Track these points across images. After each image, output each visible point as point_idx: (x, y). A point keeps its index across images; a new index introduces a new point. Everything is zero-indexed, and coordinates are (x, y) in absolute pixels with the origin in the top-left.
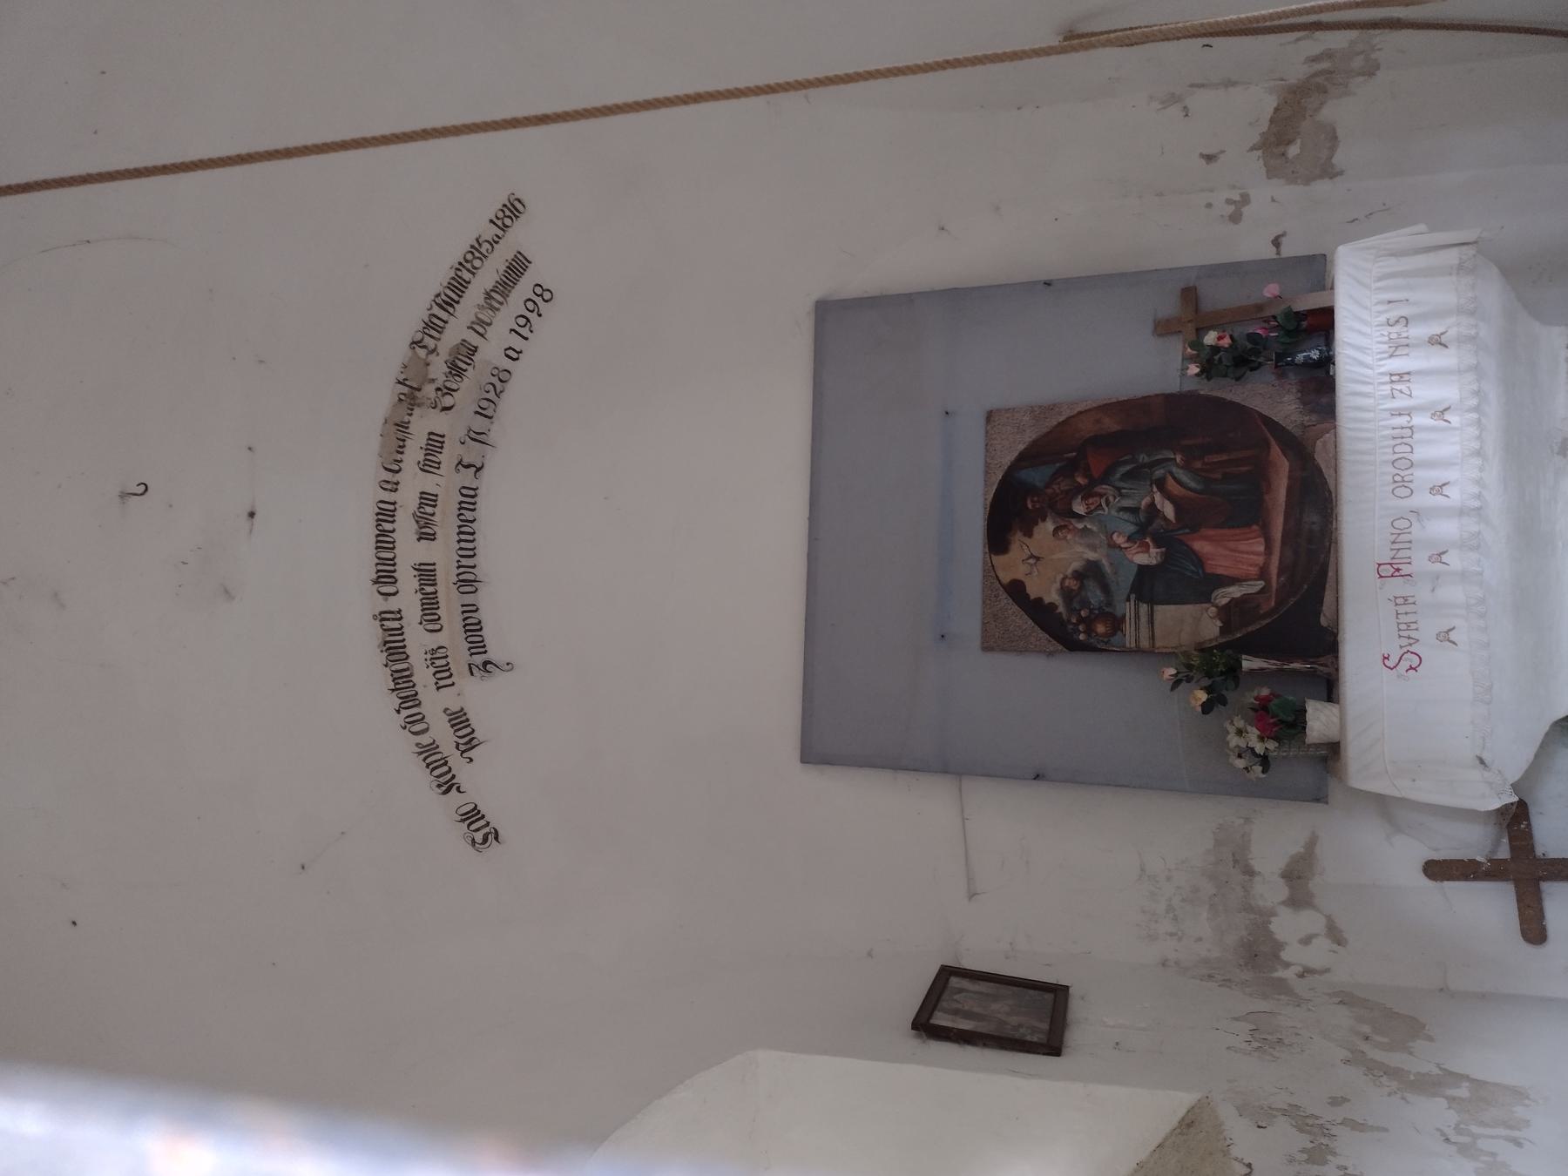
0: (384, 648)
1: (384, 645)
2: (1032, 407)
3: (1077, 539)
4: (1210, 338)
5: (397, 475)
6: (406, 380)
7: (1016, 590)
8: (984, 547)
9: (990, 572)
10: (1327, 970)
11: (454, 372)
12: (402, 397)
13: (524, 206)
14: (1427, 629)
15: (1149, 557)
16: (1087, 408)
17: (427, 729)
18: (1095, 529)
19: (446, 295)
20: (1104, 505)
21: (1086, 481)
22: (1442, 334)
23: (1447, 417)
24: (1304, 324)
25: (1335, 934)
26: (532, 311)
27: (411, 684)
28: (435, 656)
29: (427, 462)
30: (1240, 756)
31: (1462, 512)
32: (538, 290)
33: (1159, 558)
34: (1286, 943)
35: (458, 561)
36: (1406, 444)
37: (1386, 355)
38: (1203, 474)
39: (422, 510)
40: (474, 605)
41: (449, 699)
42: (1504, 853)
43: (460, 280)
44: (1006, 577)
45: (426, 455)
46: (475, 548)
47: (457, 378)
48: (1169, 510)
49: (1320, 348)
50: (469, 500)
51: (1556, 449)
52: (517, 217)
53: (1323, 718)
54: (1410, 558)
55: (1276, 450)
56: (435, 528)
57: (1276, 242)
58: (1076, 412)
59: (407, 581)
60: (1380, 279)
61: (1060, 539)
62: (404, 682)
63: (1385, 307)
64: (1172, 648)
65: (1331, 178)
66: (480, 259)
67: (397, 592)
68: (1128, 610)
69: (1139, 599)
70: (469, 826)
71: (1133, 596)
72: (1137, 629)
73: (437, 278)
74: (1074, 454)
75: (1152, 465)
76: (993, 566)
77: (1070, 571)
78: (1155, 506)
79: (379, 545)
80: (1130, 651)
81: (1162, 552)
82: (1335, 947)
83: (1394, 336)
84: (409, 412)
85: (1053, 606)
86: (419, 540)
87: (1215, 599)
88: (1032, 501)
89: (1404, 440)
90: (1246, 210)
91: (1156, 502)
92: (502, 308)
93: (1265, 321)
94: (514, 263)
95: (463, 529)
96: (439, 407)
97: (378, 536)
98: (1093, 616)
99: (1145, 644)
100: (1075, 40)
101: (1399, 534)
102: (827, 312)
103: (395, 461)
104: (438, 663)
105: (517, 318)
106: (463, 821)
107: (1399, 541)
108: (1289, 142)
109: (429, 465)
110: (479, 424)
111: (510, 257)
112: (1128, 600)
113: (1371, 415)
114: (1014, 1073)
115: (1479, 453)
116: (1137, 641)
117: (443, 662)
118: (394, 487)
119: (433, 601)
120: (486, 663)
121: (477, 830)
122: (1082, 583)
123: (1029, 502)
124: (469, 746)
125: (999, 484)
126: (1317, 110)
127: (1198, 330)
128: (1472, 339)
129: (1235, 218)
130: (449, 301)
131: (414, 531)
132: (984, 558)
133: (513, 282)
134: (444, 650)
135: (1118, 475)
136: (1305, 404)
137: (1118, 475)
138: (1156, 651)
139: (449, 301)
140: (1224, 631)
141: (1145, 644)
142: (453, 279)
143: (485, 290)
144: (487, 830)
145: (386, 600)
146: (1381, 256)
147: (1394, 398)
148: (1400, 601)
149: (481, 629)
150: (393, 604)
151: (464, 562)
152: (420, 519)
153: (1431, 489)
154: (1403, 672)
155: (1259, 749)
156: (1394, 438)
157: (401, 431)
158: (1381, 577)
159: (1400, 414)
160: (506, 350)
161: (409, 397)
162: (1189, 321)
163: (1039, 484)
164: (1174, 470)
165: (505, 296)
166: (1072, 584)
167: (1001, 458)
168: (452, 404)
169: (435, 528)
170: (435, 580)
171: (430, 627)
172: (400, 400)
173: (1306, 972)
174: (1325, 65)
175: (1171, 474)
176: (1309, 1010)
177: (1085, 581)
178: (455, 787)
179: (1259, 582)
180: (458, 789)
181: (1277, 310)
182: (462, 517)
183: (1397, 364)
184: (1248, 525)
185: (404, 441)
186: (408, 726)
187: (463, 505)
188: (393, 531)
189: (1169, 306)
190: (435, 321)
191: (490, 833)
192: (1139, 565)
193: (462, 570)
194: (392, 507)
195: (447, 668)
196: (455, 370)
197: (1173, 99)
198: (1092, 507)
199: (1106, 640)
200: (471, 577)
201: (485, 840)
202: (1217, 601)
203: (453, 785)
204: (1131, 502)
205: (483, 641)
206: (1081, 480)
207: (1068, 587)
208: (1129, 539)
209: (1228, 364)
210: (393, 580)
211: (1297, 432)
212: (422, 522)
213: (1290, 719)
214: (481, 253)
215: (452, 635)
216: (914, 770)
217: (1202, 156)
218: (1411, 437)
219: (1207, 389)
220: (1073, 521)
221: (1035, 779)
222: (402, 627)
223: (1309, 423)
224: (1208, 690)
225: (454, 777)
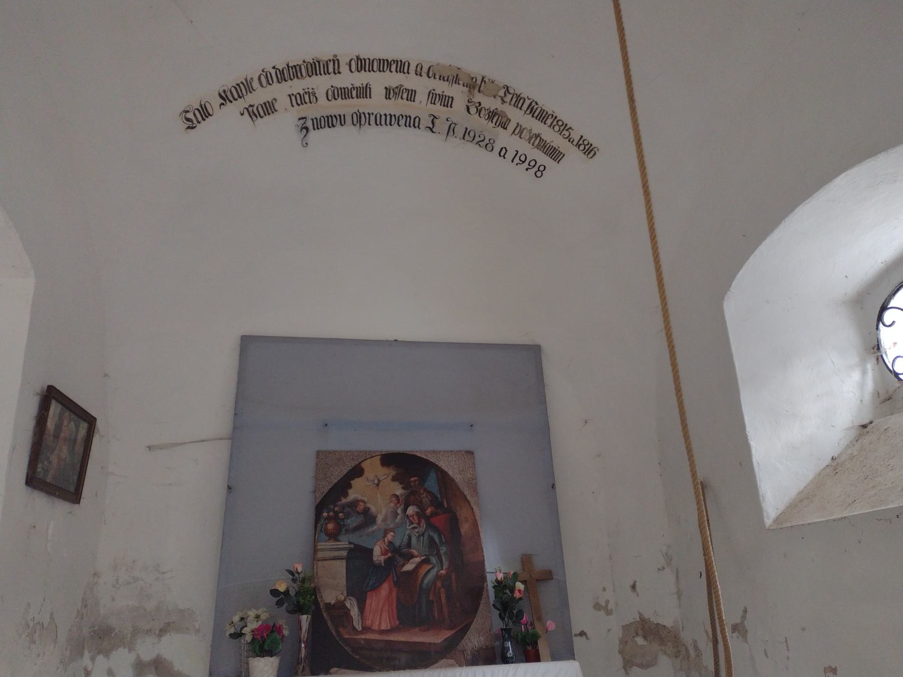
0: (315, 61)
1: (317, 61)
2: (476, 479)
3: (390, 510)
4: (520, 586)
5: (426, 75)
6: (485, 82)
7: (357, 471)
8: (385, 452)
9: (370, 455)
11: (491, 114)
12: (474, 80)
13: (592, 157)
15: (378, 556)
17: (262, 86)
18: (397, 521)
19: (537, 109)
20: (413, 526)
21: (428, 514)
24: (530, 648)
26: (529, 165)
27: (292, 78)
28: (311, 94)
29: (434, 95)
30: (242, 619)
32: (542, 168)
35: (373, 114)
39: (404, 91)
40: (345, 123)
41: (283, 102)
43: (546, 117)
44: (364, 465)
45: (439, 95)
46: (381, 125)
47: (487, 116)
48: (409, 567)
49: (514, 657)
50: (412, 122)
52: (585, 153)
53: (266, 669)
55: (448, 634)
56: (393, 99)
57: (582, 634)
58: (472, 506)
59: (360, 79)
61: (390, 499)
62: (293, 72)
64: (317, 573)
65: (624, 667)
66: (559, 130)
67: (352, 72)
68: (343, 543)
70: (198, 110)
71: (352, 546)
72: (331, 550)
73: (547, 103)
76: (373, 457)
77: (369, 505)
78: (412, 559)
79: (382, 61)
80: (315, 546)
81: (381, 563)
84: (465, 85)
85: (346, 495)
86: (386, 88)
87: (349, 599)
88: (415, 481)
92: (531, 145)
93: (531, 623)
94: (557, 152)
95: (393, 117)
96: (469, 104)
97: (387, 60)
99: (320, 555)
100: (701, 489)
102: (534, 351)
103: (435, 74)
104: (307, 97)
105: (525, 155)
106: (201, 106)
108: (645, 637)
109: (433, 97)
110: (460, 131)
111: (561, 150)
112: (350, 543)
114: (13, 448)
116: (322, 550)
117: (307, 100)
118: (418, 73)
119: (347, 95)
120: (307, 129)
121: (194, 114)
123: (415, 478)
124: (251, 114)
125: (427, 460)
126: (665, 653)
127: (526, 581)
129: (597, 607)
130: (534, 110)
131: (391, 85)
132: (379, 452)
133: (546, 152)
134: (315, 101)
135: (432, 534)
137: (432, 534)
139: (534, 110)
140: (328, 606)
141: (320, 555)
142: (547, 113)
143: (541, 134)
144: (195, 121)
145: (346, 64)
149: (329, 127)
150: (344, 68)
151: (373, 118)
152: (399, 89)
155: (246, 630)
157: (453, 78)
160: (505, 148)
161: (474, 85)
164: (435, 570)
165: (538, 147)
166: (361, 507)
167: (443, 460)
168: (471, 112)
169: (393, 99)
170: (360, 98)
171: (330, 93)
172: (472, 78)
174: (692, 653)
175: (433, 568)
176: (58, 669)
178: (223, 101)
179: (360, 626)
180: (222, 104)
181: (539, 629)
182: (401, 117)
184: (399, 618)
185: (447, 80)
186: (264, 74)
187: (408, 118)
188: (391, 71)
189: (540, 563)
190: (522, 101)
191: (193, 124)
192: (373, 549)
193: (367, 116)
194: (406, 70)
195: (303, 102)
196: (492, 115)
197: (669, 559)
198: (411, 519)
200: (363, 122)
201: (188, 120)
202: (348, 600)
203: (225, 101)
204: (414, 543)
205: (321, 128)
206: (429, 511)
207: (358, 505)
208: (390, 543)
210: (359, 70)
211: (460, 647)
212: (396, 90)
213: (266, 647)
214: (563, 130)
215: (324, 107)
216: (235, 407)
217: (635, 582)
220: (403, 506)
221: (228, 486)
222: (329, 74)
223: (466, 655)
224: (287, 592)
225: (231, 102)
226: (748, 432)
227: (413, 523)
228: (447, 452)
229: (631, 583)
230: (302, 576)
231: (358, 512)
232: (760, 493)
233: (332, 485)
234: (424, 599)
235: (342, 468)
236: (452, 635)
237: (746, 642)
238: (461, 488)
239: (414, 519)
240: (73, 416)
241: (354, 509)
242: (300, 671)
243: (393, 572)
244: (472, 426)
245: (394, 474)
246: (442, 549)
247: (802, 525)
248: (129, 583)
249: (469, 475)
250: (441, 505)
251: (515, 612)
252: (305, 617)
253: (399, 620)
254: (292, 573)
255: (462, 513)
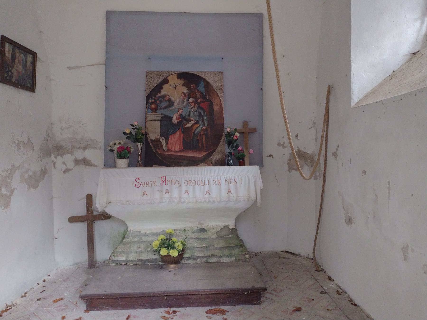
4: (237, 134)
7: (165, 81)
8: (179, 72)
9: (172, 73)
10: (55, 168)
14: (147, 189)
15: (175, 120)
16: (221, 102)
20: (192, 107)
21: (199, 102)
22: (231, 193)
23: (207, 194)
25: (66, 171)
31: (180, 198)
33: (175, 122)
34: (63, 158)
36: (200, 184)
37: (226, 179)
38: (199, 134)
42: (95, 213)
44: (169, 78)
48: (189, 125)
49: (232, 164)
51: (200, 222)
54: (167, 185)
55: (205, 153)
57: (271, 156)
60: (248, 177)
63: (240, 178)
64: (147, 126)
69: (162, 117)
71: (163, 115)
74: (208, 98)
75: (203, 121)
76: (173, 74)
77: (171, 97)
80: (146, 115)
81: (176, 123)
82: (63, 171)
83: (231, 181)
85: (160, 92)
88: (194, 86)
89: (201, 183)
90: (281, 147)
91: (192, 122)
98: (157, 104)
101: (174, 182)
107: (172, 182)
113: (209, 174)
115: (197, 202)
116: (149, 116)
122: (168, 101)
123: (193, 85)
126: (307, 164)
128: (229, 201)
129: (279, 144)
135: (200, 111)
136: (218, 161)
138: (146, 122)
140: (152, 140)
146: (255, 177)
147: (214, 180)
148: (155, 182)
153: (187, 190)
154: (134, 183)
156: (202, 181)
158: (162, 177)
159: (209, 182)
162: (246, 130)
163: (199, 88)
164: (201, 127)
166: (167, 98)
173: (54, 163)
177: (168, 102)
179: (166, 149)
181: (246, 153)
183: (223, 182)
189: (251, 125)
192: (172, 117)
199: (149, 108)
202: (161, 138)
206: (199, 101)
207: (166, 97)
208: (181, 114)
209: (229, 139)
211: (210, 159)
218: (202, 185)
219: (224, 134)
223: (212, 162)
224: (130, 133)
226: (352, 58)
227: (191, 106)
228: (210, 72)
229: (296, 135)
230: (137, 127)
231: (166, 100)
232: (352, 90)
233: (153, 88)
234: (195, 139)
235: (158, 79)
236: (207, 154)
237: (337, 160)
238: (215, 90)
239: (192, 104)
240: (21, 51)
241: (164, 98)
242: (138, 165)
243: (181, 128)
244: (222, 59)
245: (183, 83)
246: (205, 118)
247: (364, 105)
248: (68, 128)
249: (220, 84)
250: (205, 98)
251: (235, 145)
252: (139, 144)
253: (183, 147)
254: (133, 126)
255: (215, 102)
